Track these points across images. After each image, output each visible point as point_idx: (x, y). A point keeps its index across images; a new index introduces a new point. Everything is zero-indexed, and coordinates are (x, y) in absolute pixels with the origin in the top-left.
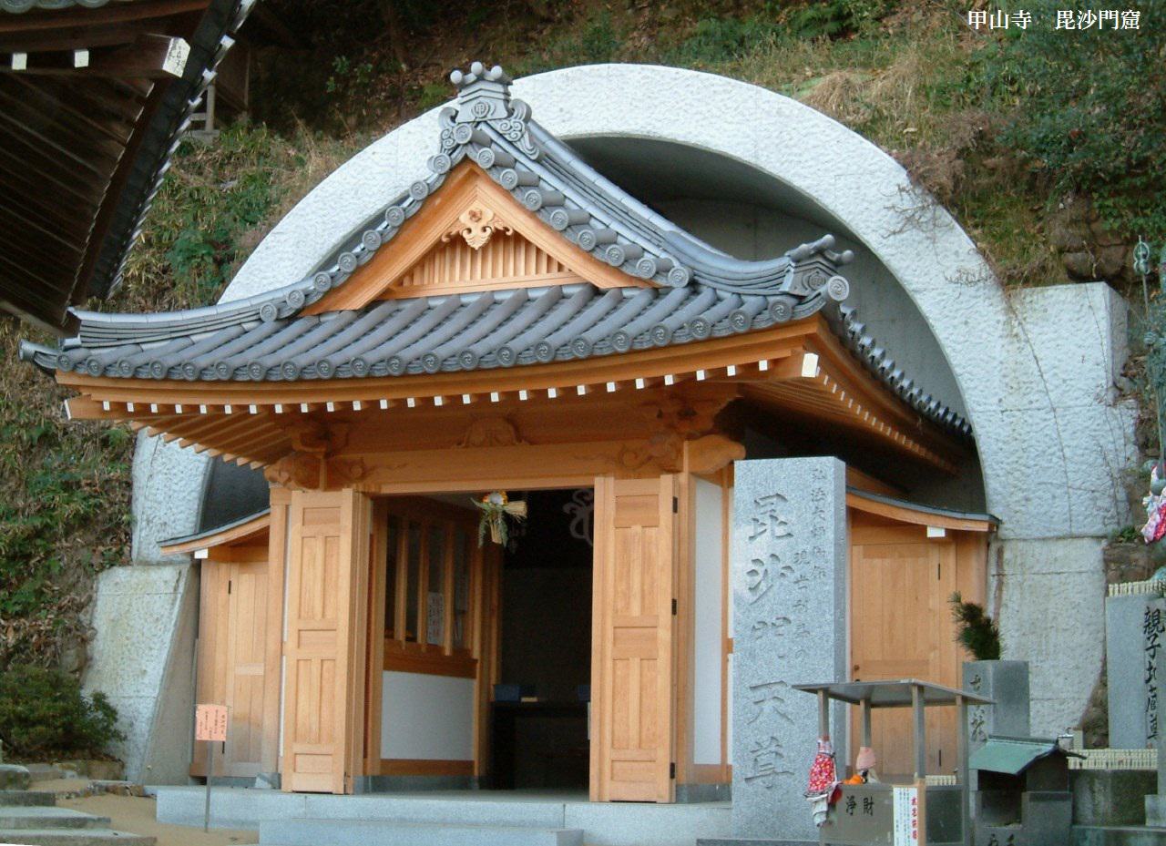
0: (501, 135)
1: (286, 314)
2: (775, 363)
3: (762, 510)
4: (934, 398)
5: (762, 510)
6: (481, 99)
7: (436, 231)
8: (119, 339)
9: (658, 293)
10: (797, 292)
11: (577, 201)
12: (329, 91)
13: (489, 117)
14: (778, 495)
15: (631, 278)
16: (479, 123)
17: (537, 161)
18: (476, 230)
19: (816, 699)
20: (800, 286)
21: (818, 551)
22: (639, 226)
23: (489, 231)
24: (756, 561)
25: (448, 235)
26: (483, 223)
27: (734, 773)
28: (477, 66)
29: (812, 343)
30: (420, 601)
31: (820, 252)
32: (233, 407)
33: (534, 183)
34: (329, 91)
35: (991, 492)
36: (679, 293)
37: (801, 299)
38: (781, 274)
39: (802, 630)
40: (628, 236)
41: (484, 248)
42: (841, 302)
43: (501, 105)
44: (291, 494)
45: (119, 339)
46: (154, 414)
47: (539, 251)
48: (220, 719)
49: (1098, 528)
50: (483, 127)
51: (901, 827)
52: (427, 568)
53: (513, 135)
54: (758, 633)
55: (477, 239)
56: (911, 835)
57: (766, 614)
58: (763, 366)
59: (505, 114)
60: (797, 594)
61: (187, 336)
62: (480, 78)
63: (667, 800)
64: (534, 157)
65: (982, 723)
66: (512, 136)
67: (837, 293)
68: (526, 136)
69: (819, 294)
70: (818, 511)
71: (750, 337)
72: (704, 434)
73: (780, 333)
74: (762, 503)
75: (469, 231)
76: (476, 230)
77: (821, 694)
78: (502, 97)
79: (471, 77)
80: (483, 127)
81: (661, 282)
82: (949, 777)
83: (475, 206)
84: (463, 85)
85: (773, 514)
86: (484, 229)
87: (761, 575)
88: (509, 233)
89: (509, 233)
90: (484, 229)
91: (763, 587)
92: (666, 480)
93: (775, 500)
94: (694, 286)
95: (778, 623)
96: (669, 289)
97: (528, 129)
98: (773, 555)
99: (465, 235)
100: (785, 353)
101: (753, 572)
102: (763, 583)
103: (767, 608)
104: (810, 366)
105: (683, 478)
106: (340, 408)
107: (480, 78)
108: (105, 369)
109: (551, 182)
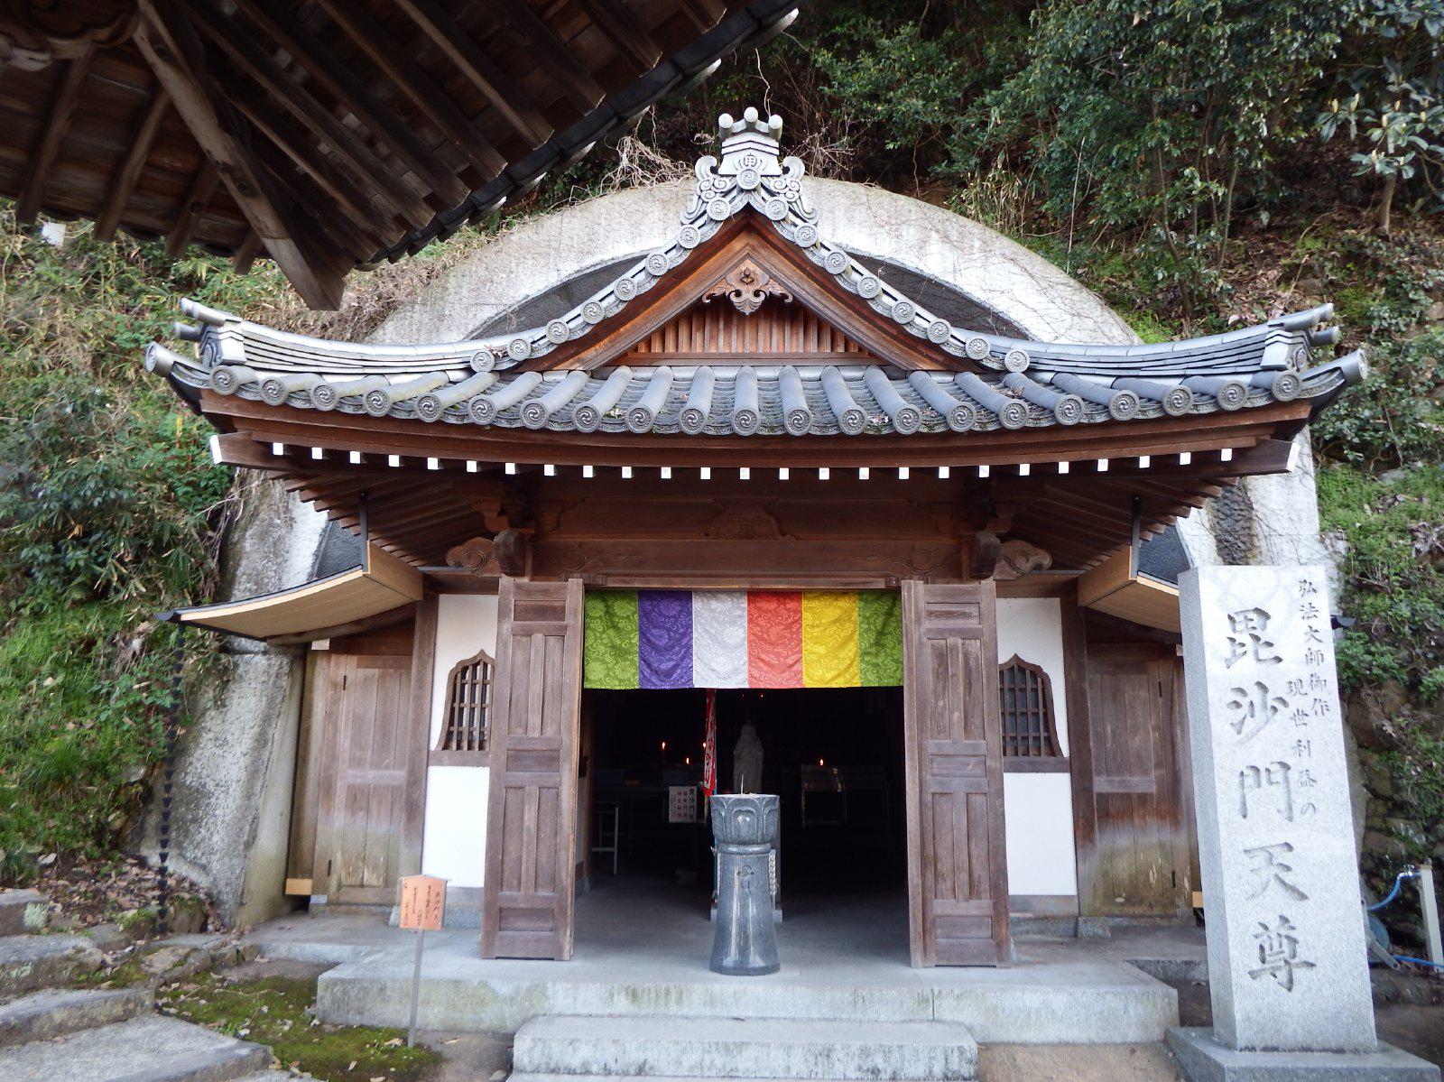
1: (505, 365)
7: (692, 291)
8: (296, 364)
18: (748, 294)
23: (762, 297)
27: (1233, 966)
28: (751, 113)
30: (1091, 728)
41: (755, 316)
44: (798, 612)
45: (296, 364)
46: (278, 457)
48: (433, 898)
49: (419, 1022)
52: (350, 733)
55: (748, 301)
61: (382, 374)
75: (738, 294)
76: (748, 294)
78: (777, 152)
86: (757, 294)
90: (757, 294)
99: (733, 298)
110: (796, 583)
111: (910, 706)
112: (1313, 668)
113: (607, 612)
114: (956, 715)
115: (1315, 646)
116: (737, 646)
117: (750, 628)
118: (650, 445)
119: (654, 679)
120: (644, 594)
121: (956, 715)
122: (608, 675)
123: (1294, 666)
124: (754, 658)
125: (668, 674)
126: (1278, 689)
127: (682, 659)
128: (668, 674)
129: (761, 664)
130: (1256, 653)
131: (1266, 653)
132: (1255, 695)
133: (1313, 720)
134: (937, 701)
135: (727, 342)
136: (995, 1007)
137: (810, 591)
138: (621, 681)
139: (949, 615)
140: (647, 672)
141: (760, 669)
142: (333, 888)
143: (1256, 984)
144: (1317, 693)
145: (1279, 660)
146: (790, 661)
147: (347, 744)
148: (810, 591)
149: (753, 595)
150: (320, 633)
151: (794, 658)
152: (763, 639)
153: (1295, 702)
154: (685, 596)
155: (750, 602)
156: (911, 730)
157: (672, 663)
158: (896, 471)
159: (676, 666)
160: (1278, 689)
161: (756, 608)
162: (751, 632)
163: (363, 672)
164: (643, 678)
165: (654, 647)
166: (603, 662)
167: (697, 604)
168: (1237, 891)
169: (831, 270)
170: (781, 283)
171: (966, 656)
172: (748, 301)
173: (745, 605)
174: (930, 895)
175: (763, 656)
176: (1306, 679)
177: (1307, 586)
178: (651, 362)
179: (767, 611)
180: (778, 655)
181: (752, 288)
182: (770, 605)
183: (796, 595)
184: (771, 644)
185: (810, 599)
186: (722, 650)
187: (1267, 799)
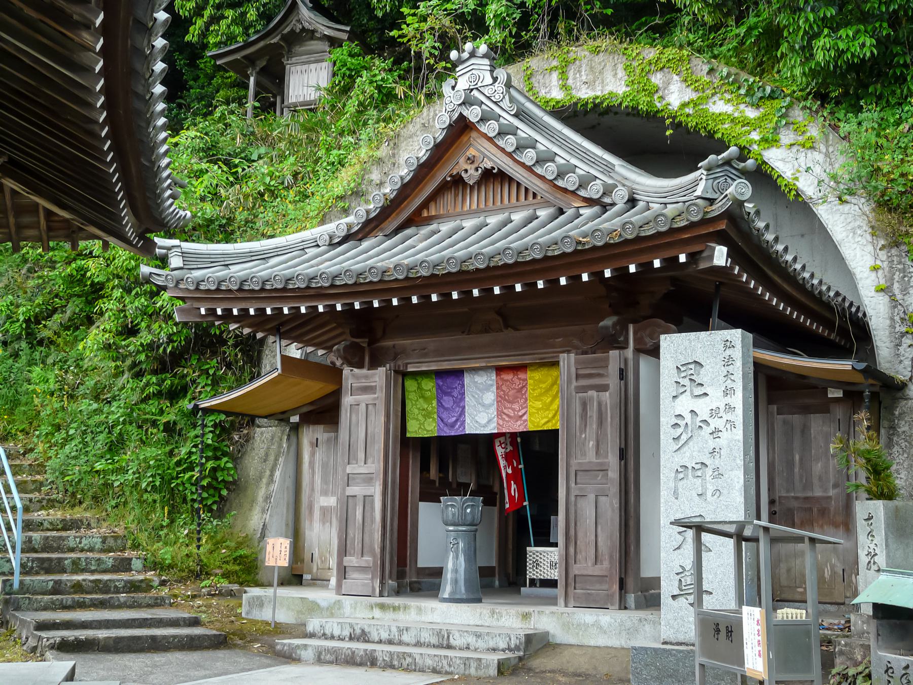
0: (489, 98)
2: (691, 256)
3: (683, 375)
4: (816, 275)
5: (683, 375)
6: (473, 71)
7: (442, 174)
9: (605, 208)
10: (708, 196)
11: (544, 144)
12: (188, 38)
13: (480, 84)
14: (695, 362)
15: (585, 200)
16: (472, 90)
17: (516, 116)
18: (471, 171)
19: (690, 533)
20: (710, 190)
21: (729, 408)
22: (573, 150)
23: (480, 171)
24: (679, 416)
25: (451, 176)
26: (476, 165)
29: (722, 238)
31: (728, 162)
32: (306, 308)
33: (513, 131)
34: (188, 38)
35: (882, 361)
36: (620, 206)
37: (711, 201)
38: (696, 183)
39: (716, 473)
40: (583, 168)
41: (479, 183)
42: (745, 201)
43: (488, 74)
47: (519, 184)
50: (475, 93)
51: (749, 645)
53: (497, 97)
54: (681, 476)
55: (472, 176)
56: (757, 653)
57: (686, 459)
58: (682, 258)
59: (491, 81)
60: (711, 444)
62: (473, 55)
63: (312, 661)
64: (513, 113)
65: (876, 554)
66: (497, 98)
67: (742, 194)
68: (507, 97)
69: (726, 196)
70: (728, 375)
71: (671, 237)
72: (646, 318)
73: (702, 232)
74: (682, 369)
75: (466, 171)
76: (471, 171)
77: (694, 529)
78: (489, 68)
79: (465, 55)
80: (475, 93)
81: (607, 200)
82: (799, 611)
83: (472, 152)
84: (460, 61)
85: (692, 377)
86: (477, 169)
87: (683, 427)
88: (494, 171)
89: (494, 171)
90: (477, 169)
91: (684, 437)
92: (614, 354)
93: (692, 366)
94: (632, 202)
95: (697, 467)
96: (613, 204)
97: (509, 93)
98: (692, 411)
99: (463, 175)
100: (696, 248)
101: (676, 425)
102: (684, 434)
103: (688, 454)
104: (720, 256)
105: (630, 352)
106: (384, 304)
107: (473, 55)
108: (198, 284)
109: (525, 131)
110: (511, 361)
111: (563, 439)
112: (728, 400)
113: (418, 388)
114: (591, 443)
115: (729, 384)
116: (491, 405)
117: (497, 393)
118: (412, 283)
119: (445, 429)
120: (439, 374)
121: (591, 443)
122: (420, 428)
123: (716, 399)
124: (500, 413)
125: (452, 426)
126: (704, 414)
127: (460, 415)
128: (452, 426)
129: (504, 416)
130: (691, 391)
131: (699, 391)
132: (688, 417)
133: (724, 435)
134: (581, 434)
135: (472, 201)
136: (568, 622)
137: (531, 365)
138: (428, 431)
139: (590, 376)
140: (442, 425)
141: (503, 420)
142: (315, 570)
143: (674, 603)
144: (729, 416)
145: (706, 394)
146: (520, 414)
147: (319, 481)
148: (531, 365)
149: (499, 370)
150: (293, 411)
151: (523, 411)
152: (505, 400)
153: (715, 423)
154: (458, 374)
155: (497, 375)
156: (562, 454)
157: (454, 419)
158: (536, 284)
159: (457, 421)
160: (704, 414)
161: (502, 379)
162: (498, 396)
163: (326, 435)
164: (439, 429)
165: (442, 406)
166: (417, 420)
167: (467, 379)
168: (668, 545)
169: (363, 220)
170: (490, 160)
171: (600, 404)
172: (472, 176)
173: (494, 377)
174: (572, 561)
175: (505, 411)
176: (722, 407)
177: (728, 344)
178: (429, 220)
179: (507, 381)
180: (514, 410)
181: (474, 166)
182: (508, 376)
183: (523, 368)
184: (509, 402)
185: (531, 370)
186: (482, 410)
187: (691, 484)
